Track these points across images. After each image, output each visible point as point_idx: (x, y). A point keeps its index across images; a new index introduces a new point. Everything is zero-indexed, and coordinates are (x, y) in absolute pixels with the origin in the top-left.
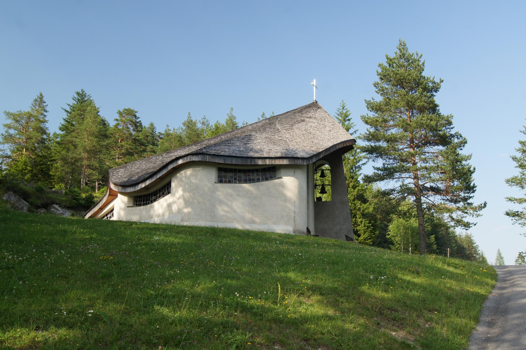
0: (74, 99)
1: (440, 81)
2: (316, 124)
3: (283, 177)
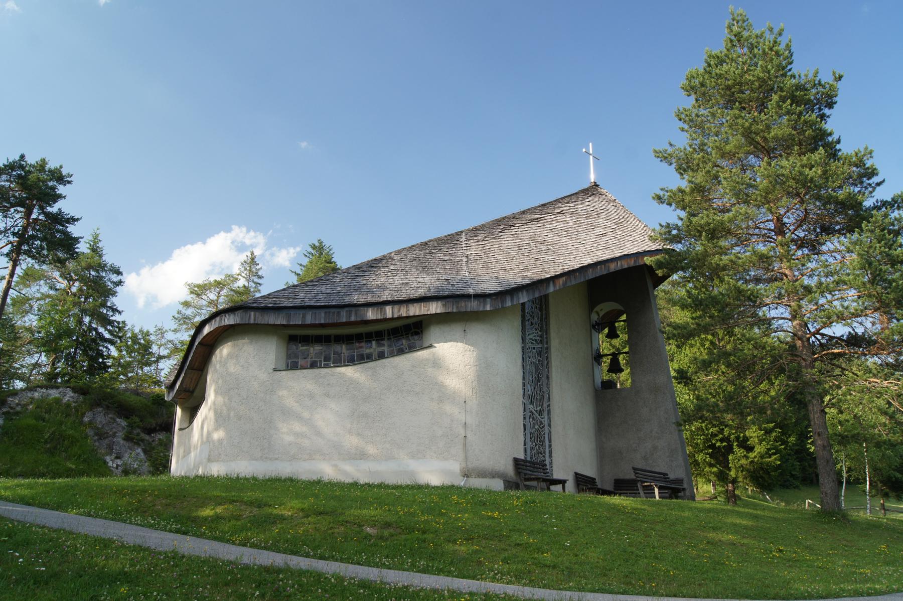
0: (308, 255)
1: (833, 78)
2: (571, 224)
3: (435, 345)
